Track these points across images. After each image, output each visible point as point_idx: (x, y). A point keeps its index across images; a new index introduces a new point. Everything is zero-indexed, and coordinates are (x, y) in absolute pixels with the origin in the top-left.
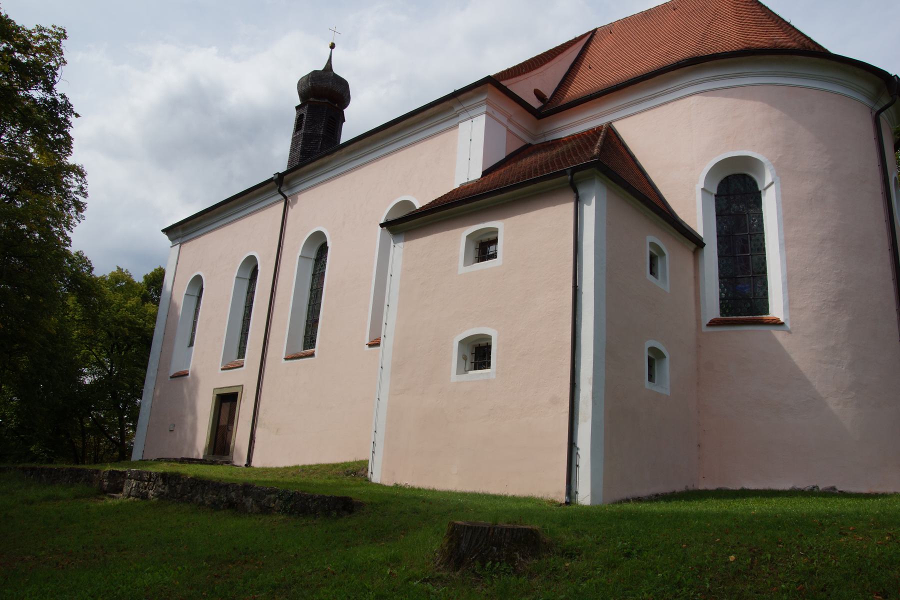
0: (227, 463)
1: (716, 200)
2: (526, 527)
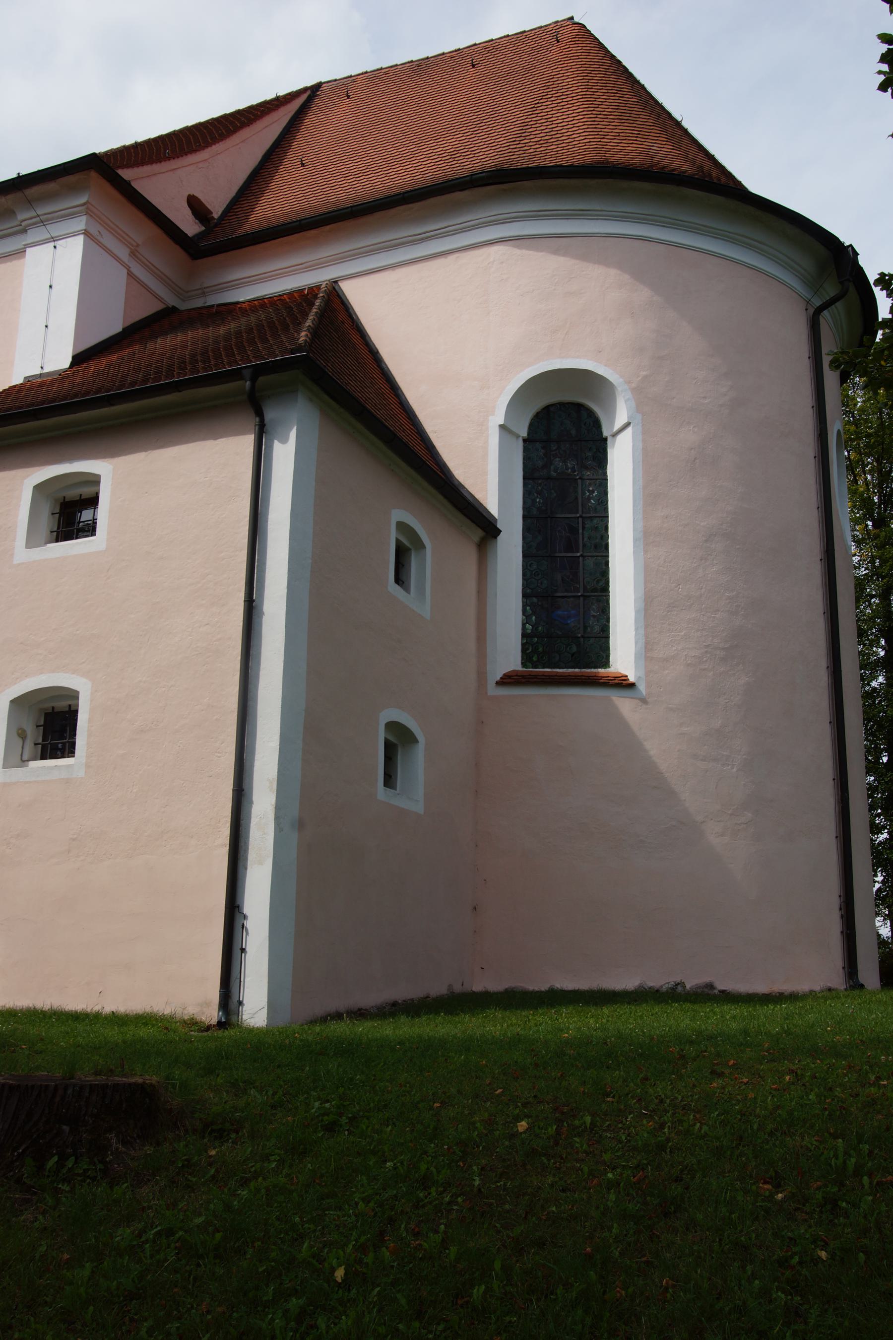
1: (525, 450)
2: (132, 1080)
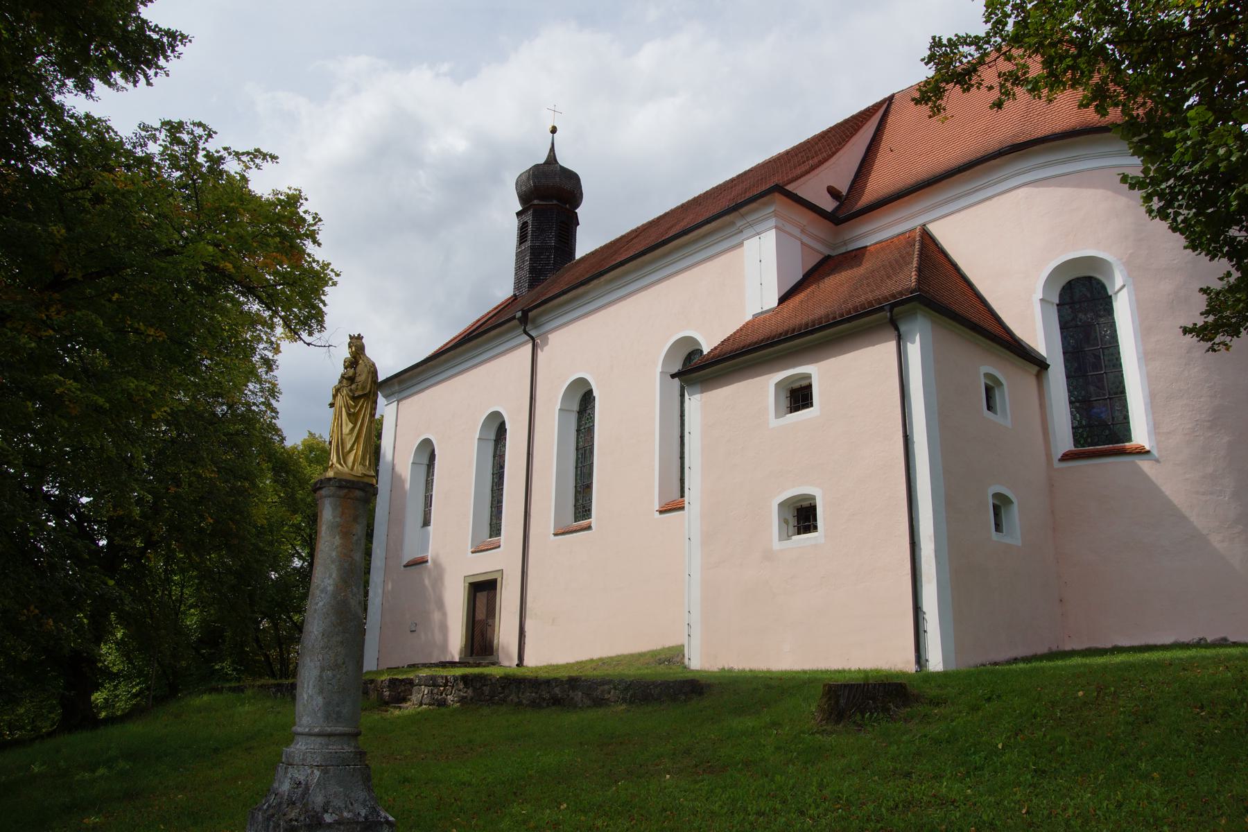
0: (493, 664)
1: (1059, 311)
